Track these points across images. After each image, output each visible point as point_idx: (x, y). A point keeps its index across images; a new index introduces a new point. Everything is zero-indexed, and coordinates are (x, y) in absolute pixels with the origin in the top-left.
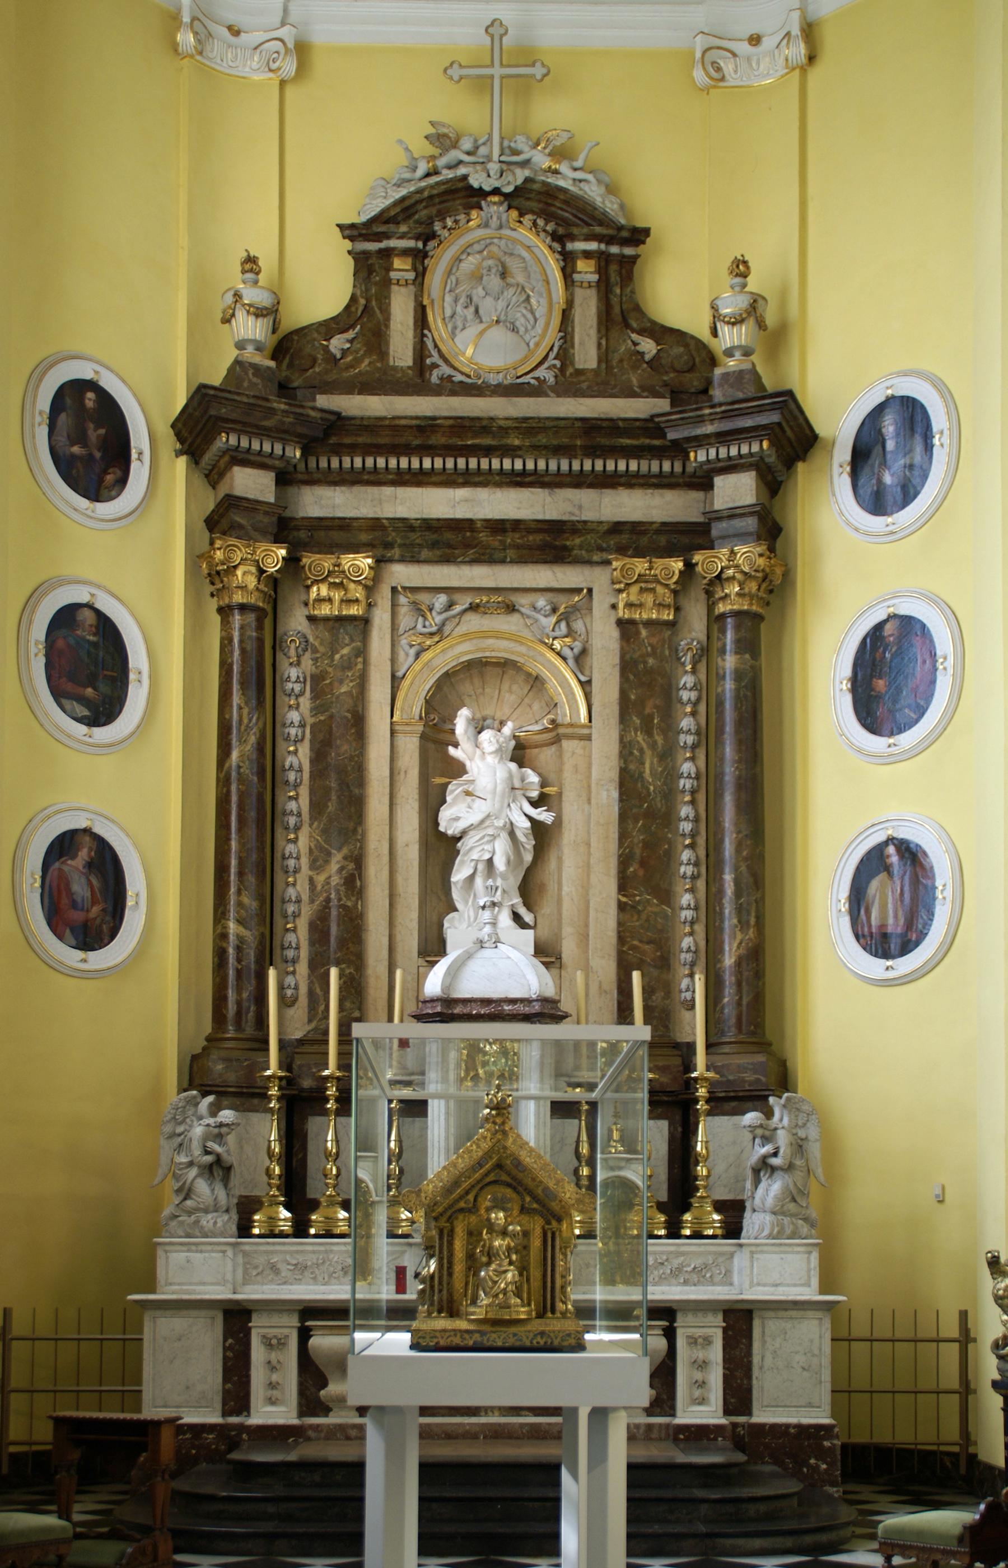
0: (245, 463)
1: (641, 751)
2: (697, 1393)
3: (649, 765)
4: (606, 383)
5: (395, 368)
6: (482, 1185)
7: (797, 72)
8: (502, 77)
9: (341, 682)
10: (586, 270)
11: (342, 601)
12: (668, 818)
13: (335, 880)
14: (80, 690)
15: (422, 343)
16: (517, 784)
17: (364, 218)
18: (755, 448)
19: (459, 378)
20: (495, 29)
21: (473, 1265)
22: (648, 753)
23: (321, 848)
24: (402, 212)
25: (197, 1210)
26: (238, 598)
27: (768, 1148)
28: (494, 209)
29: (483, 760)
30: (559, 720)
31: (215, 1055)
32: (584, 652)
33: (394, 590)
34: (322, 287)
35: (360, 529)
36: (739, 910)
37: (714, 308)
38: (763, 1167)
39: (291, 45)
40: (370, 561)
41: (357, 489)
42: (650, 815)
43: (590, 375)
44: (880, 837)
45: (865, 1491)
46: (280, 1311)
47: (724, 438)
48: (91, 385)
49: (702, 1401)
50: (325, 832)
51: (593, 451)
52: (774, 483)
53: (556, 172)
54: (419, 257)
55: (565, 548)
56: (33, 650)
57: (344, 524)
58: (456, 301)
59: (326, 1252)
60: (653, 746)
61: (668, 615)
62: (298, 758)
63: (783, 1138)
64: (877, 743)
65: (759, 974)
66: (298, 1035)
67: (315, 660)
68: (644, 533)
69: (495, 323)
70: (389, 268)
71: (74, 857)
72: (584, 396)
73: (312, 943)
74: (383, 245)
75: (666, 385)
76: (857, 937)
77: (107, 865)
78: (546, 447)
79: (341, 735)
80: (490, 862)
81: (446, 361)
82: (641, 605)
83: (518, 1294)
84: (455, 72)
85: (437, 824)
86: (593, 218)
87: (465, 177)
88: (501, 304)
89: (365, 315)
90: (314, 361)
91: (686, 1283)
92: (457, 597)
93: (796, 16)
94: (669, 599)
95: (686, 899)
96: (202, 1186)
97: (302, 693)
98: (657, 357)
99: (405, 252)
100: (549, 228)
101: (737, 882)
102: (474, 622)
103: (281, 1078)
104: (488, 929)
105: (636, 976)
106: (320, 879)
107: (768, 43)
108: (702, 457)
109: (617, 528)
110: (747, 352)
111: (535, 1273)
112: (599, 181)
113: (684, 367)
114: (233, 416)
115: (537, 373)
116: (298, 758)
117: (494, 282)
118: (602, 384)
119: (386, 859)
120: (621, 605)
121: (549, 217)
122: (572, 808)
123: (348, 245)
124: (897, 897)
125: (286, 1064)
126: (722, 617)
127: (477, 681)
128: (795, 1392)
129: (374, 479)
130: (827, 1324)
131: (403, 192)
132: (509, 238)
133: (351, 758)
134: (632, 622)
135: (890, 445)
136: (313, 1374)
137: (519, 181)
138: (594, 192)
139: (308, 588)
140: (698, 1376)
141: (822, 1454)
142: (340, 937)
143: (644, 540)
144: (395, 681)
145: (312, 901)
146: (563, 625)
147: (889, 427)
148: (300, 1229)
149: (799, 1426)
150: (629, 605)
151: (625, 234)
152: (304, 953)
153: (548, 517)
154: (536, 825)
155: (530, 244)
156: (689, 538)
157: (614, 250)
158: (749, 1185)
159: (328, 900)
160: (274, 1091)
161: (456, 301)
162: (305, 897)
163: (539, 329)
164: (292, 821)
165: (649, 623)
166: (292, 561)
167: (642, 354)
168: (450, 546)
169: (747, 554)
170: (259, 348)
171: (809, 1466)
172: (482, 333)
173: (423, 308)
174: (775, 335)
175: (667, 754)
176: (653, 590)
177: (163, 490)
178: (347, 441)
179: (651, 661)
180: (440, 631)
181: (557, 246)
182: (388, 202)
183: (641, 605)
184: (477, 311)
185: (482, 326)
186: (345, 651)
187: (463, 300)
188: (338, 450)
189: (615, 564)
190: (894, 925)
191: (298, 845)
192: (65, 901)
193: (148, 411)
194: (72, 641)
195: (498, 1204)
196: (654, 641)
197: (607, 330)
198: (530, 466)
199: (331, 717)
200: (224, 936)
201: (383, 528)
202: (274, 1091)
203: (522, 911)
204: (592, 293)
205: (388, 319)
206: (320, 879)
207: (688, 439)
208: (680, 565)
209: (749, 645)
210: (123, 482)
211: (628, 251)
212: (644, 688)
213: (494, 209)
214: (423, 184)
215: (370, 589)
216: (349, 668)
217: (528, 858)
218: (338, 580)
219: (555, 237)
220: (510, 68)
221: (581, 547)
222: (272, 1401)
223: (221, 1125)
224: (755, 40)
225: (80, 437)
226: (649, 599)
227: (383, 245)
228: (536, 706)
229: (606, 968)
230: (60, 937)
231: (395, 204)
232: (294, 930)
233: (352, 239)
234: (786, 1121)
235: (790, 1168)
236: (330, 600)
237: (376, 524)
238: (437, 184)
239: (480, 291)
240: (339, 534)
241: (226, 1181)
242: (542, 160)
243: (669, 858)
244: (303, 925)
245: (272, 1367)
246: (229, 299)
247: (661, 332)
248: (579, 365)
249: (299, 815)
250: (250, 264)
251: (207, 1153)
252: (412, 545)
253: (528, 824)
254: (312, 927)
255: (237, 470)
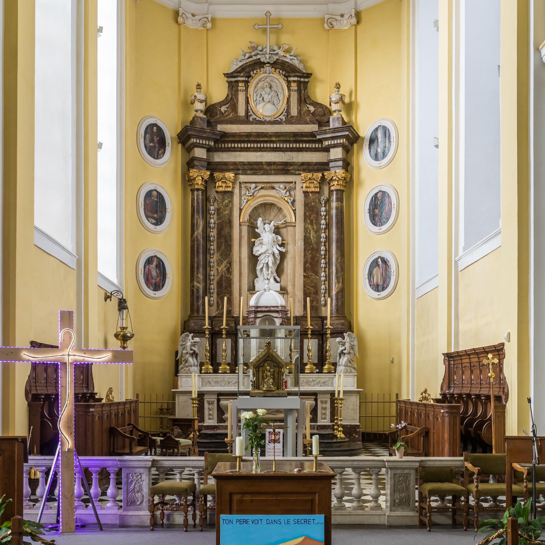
0: (198, 147)
1: (310, 230)
2: (323, 416)
3: (312, 234)
4: (300, 120)
5: (240, 116)
6: (265, 361)
7: (354, 27)
8: (270, 28)
9: (225, 210)
10: (294, 86)
11: (225, 187)
12: (318, 250)
13: (224, 269)
14: (153, 215)
15: (248, 109)
16: (275, 240)
17: (231, 71)
18: (342, 141)
19: (258, 119)
20: (268, 13)
21: (263, 379)
22: (312, 231)
23: (220, 260)
24: (237, 72)
25: (189, 366)
26: (196, 187)
27: (343, 348)
28: (268, 68)
29: (267, 236)
30: (287, 221)
31: (192, 321)
32: (294, 201)
33: (240, 183)
34: (218, 92)
35: (230, 165)
36: (337, 278)
37: (331, 99)
38: (342, 353)
39: (210, 19)
40: (233, 175)
41: (229, 153)
42: (313, 249)
43: (295, 118)
44: (376, 256)
45: (368, 444)
46: (212, 394)
47: (333, 138)
48: (155, 125)
49: (325, 419)
50: (221, 255)
51: (296, 142)
52: (347, 150)
53: (285, 57)
54: (247, 83)
55: (288, 170)
56: (140, 204)
57: (226, 164)
58: (257, 95)
59: (224, 378)
60: (313, 229)
61: (317, 190)
62: (213, 233)
63: (347, 345)
64: (376, 229)
65: (343, 296)
66: (214, 315)
67: (218, 204)
68: (311, 165)
69: (268, 101)
70: (238, 86)
71: (152, 264)
72: (293, 124)
73: (218, 288)
74: (236, 79)
75: (317, 120)
76: (370, 286)
77: (161, 267)
78: (283, 141)
79: (225, 226)
80: (267, 263)
81: (254, 114)
82: (310, 187)
83: (273, 385)
84: (257, 27)
85: (252, 252)
86: (296, 70)
87: (259, 59)
88: (270, 97)
89: (231, 101)
90: (217, 114)
91: (321, 386)
92: (258, 185)
93: (353, 10)
94: (318, 185)
95: (323, 274)
96: (190, 359)
97: (214, 214)
98: (314, 112)
99: (242, 81)
100: (284, 73)
101: (337, 269)
102: (263, 192)
103: (209, 329)
104: (267, 286)
105: (308, 299)
106: (220, 269)
107: (346, 16)
108: (327, 144)
109: (303, 164)
110: (340, 111)
111: (276, 380)
112: (298, 59)
113: (322, 115)
114: (195, 134)
115: (280, 117)
116: (213, 233)
117: (268, 90)
118: (299, 120)
119: (238, 263)
120: (304, 187)
121: (283, 70)
122: (290, 248)
123: (226, 79)
124: (382, 274)
125: (211, 324)
126: (332, 191)
127: (264, 209)
128: (350, 415)
129: (234, 150)
130: (358, 397)
131: (242, 63)
132: (272, 76)
133: (228, 233)
134: (307, 192)
135: (380, 140)
136: (221, 411)
137: (275, 60)
138: (296, 63)
139: (216, 183)
140: (324, 411)
141: (357, 433)
142: (225, 286)
143: (311, 167)
144: (241, 210)
145: (218, 275)
146: (288, 193)
147: (380, 134)
148: (216, 371)
149: (350, 425)
150: (307, 187)
151: (305, 75)
152: (216, 291)
153: (283, 161)
154: (281, 253)
155: (278, 79)
156: (324, 167)
157: (302, 80)
158: (338, 358)
159: (222, 275)
160: (207, 332)
161: (257, 95)
162: (216, 274)
163: (281, 104)
164: (212, 252)
165: (312, 192)
166: (212, 175)
167: (310, 111)
168: (256, 170)
169: (340, 172)
170: (201, 111)
171: (353, 436)
172: (264, 105)
173: (248, 98)
174: (349, 107)
175: (318, 231)
176: (313, 183)
177: (172, 156)
178: (226, 139)
179: (313, 203)
180: (253, 194)
181: (286, 79)
182: (238, 67)
183: (310, 187)
184: (263, 99)
185: (264, 103)
186: (226, 201)
187: (259, 95)
188: (224, 142)
189: (302, 175)
190: (380, 283)
191: (214, 259)
192: (150, 277)
193: (170, 133)
194: (151, 201)
195: (268, 365)
196: (313, 197)
197: (300, 104)
198: (278, 146)
199: (223, 221)
200: (193, 286)
201: (237, 164)
202: (207, 332)
203: (277, 277)
204: (296, 93)
205: (238, 101)
206: (220, 269)
207: (323, 138)
208: (321, 175)
209: (340, 199)
210: (164, 153)
211: (306, 80)
212: (311, 212)
213: (268, 68)
214: (247, 61)
215: (234, 183)
216: (227, 206)
217: (278, 262)
218: (224, 180)
219: (285, 76)
220: (271, 25)
221: (293, 170)
222: (210, 419)
223: (195, 342)
224: (342, 16)
225: (152, 141)
226: (312, 185)
227: (236, 79)
228: (280, 216)
229: (300, 294)
230: (149, 288)
231: (239, 67)
232: (213, 284)
233: (227, 77)
234: (348, 340)
235: (349, 353)
236: (222, 186)
237: (235, 163)
238: (252, 61)
239: (264, 93)
240: (224, 167)
241: (196, 358)
242: (281, 53)
243: (318, 262)
244: (215, 282)
245: (210, 409)
246: (193, 97)
247: (316, 104)
248: (292, 115)
249: (214, 250)
250: (199, 86)
251: (191, 350)
252: (245, 170)
253: (278, 252)
254: (218, 283)
255: (195, 149)
